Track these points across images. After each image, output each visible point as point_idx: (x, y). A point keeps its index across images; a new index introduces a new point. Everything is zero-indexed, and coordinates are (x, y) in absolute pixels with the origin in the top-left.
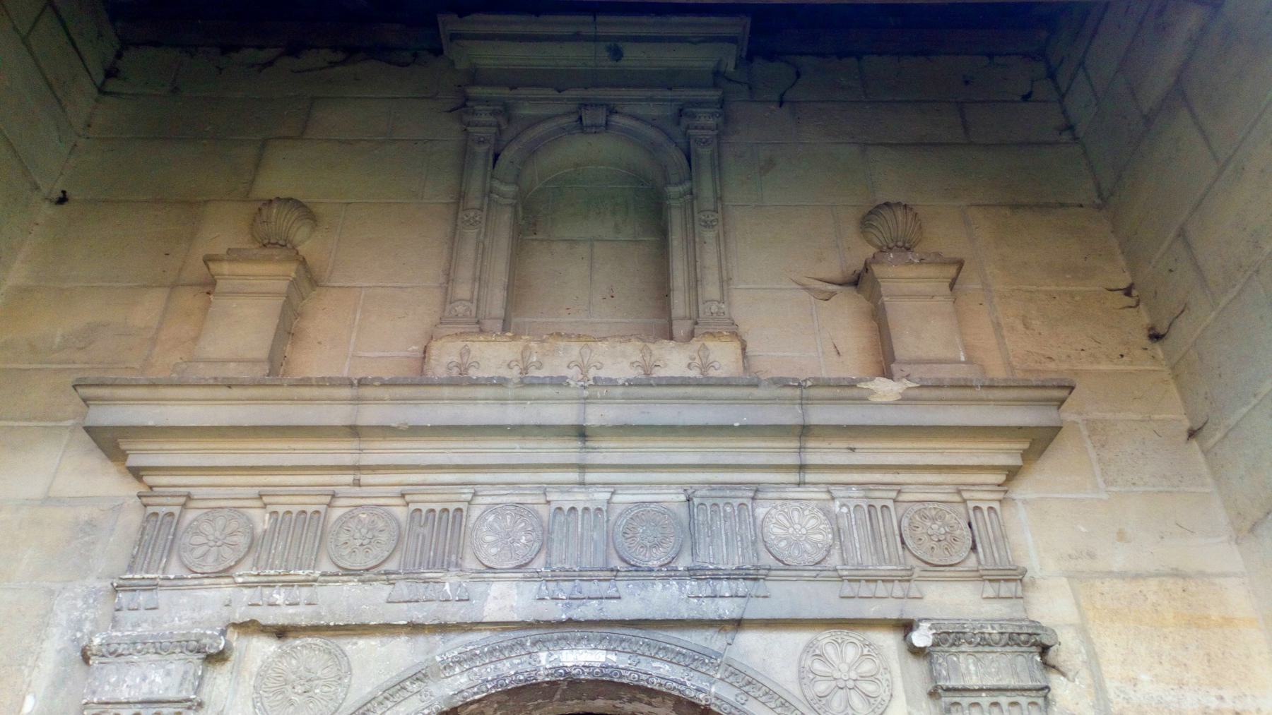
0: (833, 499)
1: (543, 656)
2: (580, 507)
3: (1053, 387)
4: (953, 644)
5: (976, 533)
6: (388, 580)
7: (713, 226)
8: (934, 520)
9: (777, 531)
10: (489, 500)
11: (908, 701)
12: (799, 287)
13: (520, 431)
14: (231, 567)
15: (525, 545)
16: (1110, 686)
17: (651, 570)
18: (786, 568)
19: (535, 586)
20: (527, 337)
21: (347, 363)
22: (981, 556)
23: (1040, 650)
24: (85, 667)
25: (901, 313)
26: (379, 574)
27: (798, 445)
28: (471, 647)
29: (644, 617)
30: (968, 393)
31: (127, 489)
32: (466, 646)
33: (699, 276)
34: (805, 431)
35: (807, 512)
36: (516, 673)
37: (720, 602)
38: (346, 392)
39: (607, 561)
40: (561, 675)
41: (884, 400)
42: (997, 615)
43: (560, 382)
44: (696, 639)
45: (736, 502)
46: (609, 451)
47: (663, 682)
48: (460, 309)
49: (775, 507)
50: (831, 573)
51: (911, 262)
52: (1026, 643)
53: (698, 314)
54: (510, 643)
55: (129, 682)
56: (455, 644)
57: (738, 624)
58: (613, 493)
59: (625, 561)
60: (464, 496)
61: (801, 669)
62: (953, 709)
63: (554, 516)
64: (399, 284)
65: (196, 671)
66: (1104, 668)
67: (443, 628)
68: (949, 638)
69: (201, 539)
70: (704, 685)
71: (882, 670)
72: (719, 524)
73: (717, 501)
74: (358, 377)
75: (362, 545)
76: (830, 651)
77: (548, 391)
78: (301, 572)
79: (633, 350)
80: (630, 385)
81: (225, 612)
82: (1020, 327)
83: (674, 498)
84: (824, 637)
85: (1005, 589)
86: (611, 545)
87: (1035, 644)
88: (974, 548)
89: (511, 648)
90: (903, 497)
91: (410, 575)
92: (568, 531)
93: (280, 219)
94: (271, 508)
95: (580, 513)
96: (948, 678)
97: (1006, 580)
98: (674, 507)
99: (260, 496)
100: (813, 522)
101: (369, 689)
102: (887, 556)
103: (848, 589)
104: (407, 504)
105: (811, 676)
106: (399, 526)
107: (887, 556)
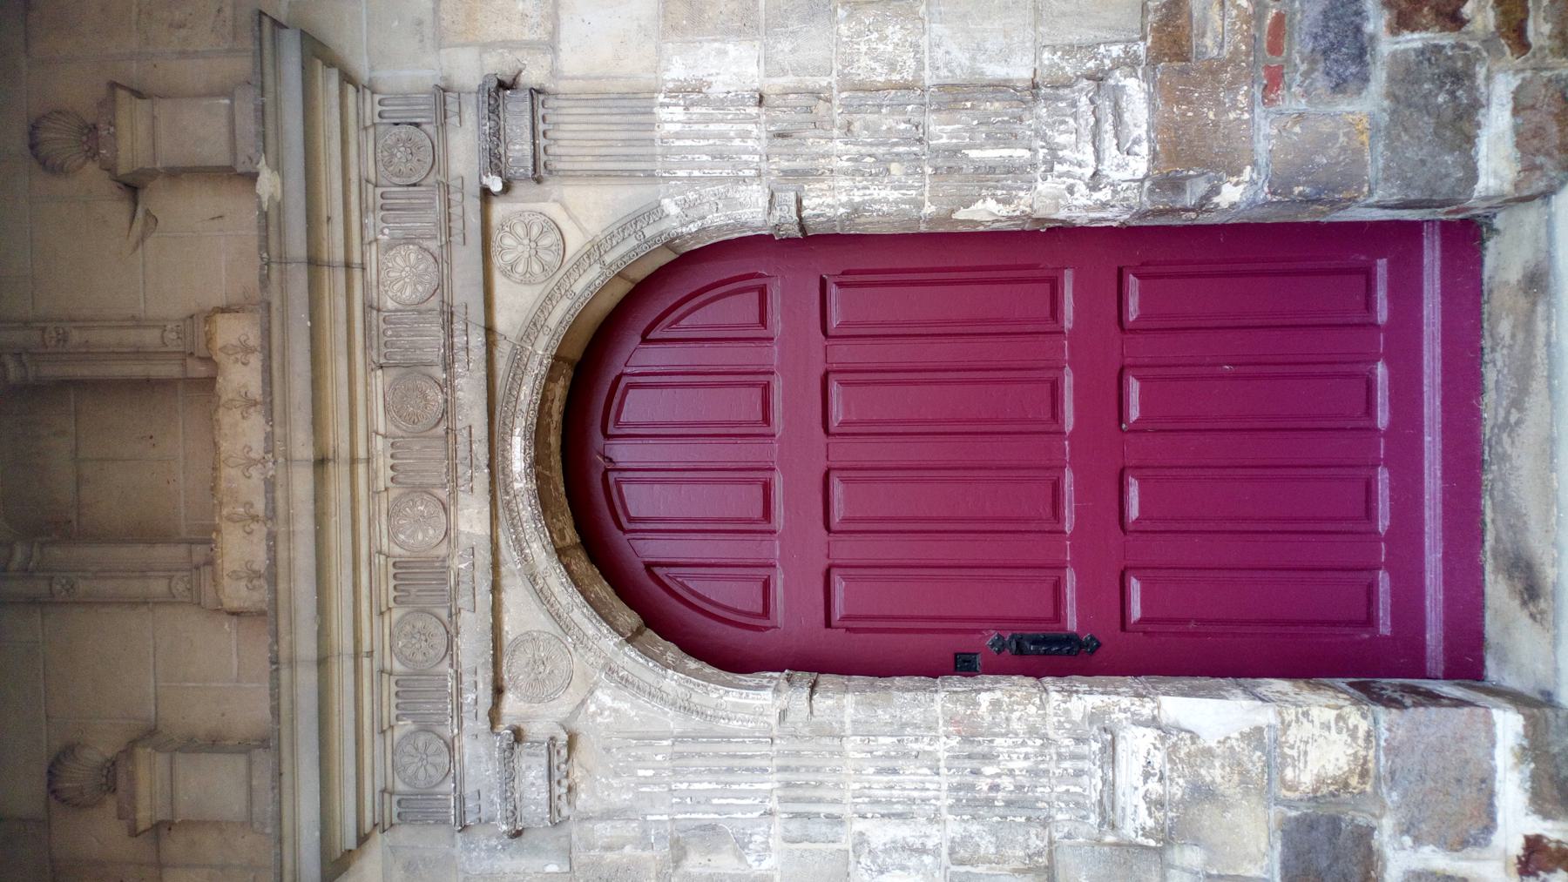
0: (376, 240)
1: (517, 486)
2: (391, 462)
3: (261, 31)
4: (499, 159)
5: (403, 120)
6: (456, 614)
7: (64, 333)
8: (392, 155)
9: (408, 292)
10: (385, 540)
11: (545, 201)
12: (140, 247)
13: (320, 518)
14: (445, 742)
15: (426, 506)
16: (528, 36)
17: (446, 401)
18: (442, 286)
19: (461, 495)
20: (217, 518)
21: (248, 686)
22: (424, 120)
23: (501, 90)
24: (525, 834)
25: (171, 153)
26: (451, 622)
27: (326, 268)
28: (511, 543)
29: (485, 407)
30: (269, 109)
31: (378, 843)
32: (509, 546)
33: (132, 349)
34: (314, 262)
35: (390, 265)
36: (530, 506)
37: (471, 345)
38: (285, 674)
39: (439, 437)
40: (531, 471)
41: (279, 186)
42: (474, 118)
43: (270, 485)
44: (502, 365)
45: (383, 326)
46: (338, 437)
47: (535, 391)
48: (180, 587)
49: (386, 292)
50: (444, 251)
51: (114, 135)
52: (496, 100)
53: (179, 352)
54: (507, 512)
55: (535, 795)
56: (508, 554)
57: (489, 330)
58: (377, 433)
59: (439, 422)
60: (382, 562)
61: (523, 283)
62: (549, 167)
63: (400, 483)
64: (151, 650)
65: (528, 747)
66: (515, 38)
67: (495, 566)
68: (495, 163)
69: (422, 773)
70: (537, 359)
71: (522, 219)
72: (405, 340)
73: (382, 342)
74: (268, 664)
75: (426, 641)
76: (508, 257)
77: (279, 494)
78: (450, 684)
79: (227, 418)
80: (272, 420)
81: (482, 737)
82: (183, 32)
83: (379, 380)
84: (497, 261)
85: (452, 108)
86: (424, 434)
87: (497, 92)
88: (417, 125)
89: (511, 511)
90: (372, 177)
91: (453, 597)
92: (412, 471)
93: (77, 776)
94: (393, 721)
95: (396, 461)
96: (526, 168)
97: (445, 104)
98: (388, 380)
99: (383, 732)
100: (399, 260)
101: (542, 616)
102: (427, 201)
103: (457, 239)
104: (389, 609)
105: (528, 275)
106: (409, 613)
107: (427, 201)
